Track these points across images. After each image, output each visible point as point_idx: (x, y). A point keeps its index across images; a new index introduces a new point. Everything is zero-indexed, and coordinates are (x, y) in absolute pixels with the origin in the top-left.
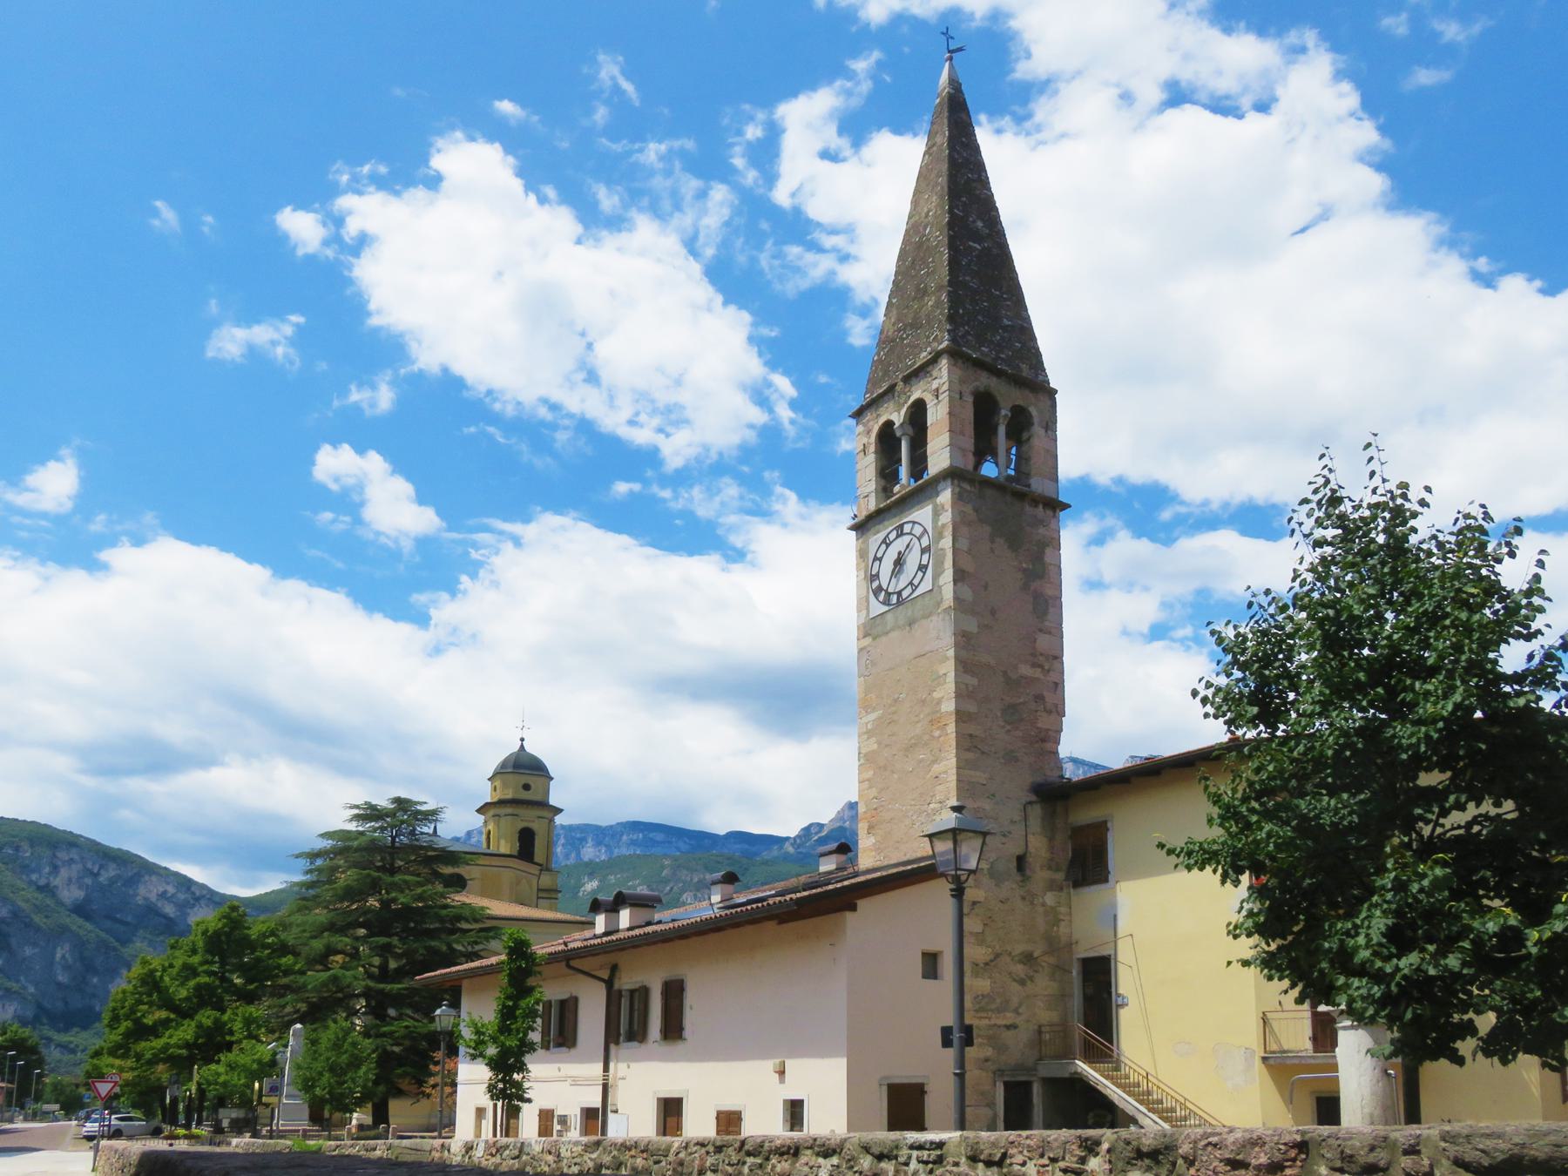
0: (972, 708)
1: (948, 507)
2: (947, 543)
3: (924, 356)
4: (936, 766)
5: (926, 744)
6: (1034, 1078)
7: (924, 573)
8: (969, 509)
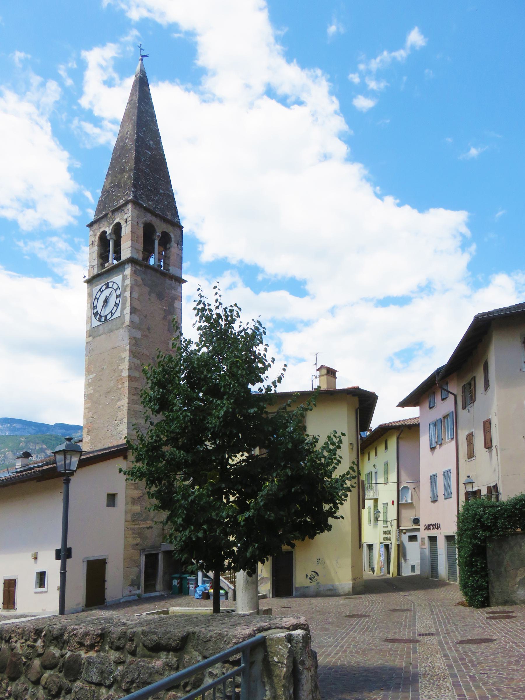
0: (137, 374)
1: (129, 276)
2: (128, 294)
3: (122, 202)
6: (160, 551)
7: (117, 308)
8: (139, 279)
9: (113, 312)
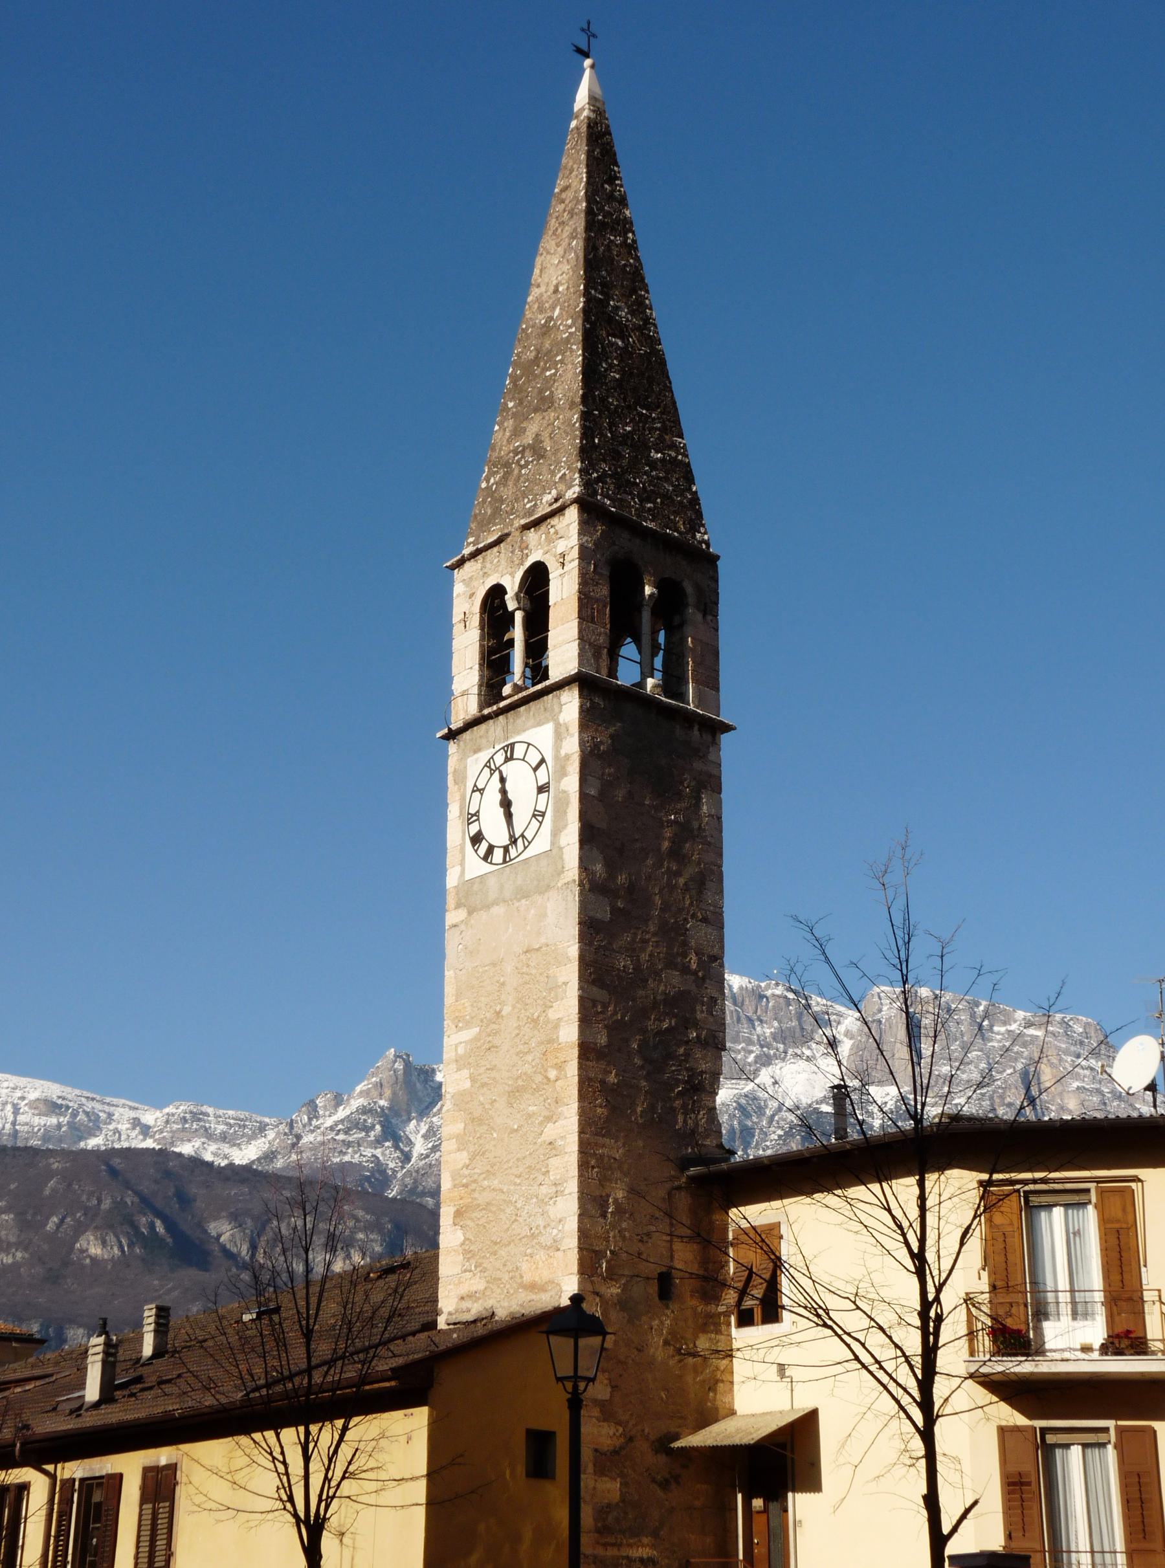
2: (571, 784)
4: (550, 1125)
5: (537, 1090)
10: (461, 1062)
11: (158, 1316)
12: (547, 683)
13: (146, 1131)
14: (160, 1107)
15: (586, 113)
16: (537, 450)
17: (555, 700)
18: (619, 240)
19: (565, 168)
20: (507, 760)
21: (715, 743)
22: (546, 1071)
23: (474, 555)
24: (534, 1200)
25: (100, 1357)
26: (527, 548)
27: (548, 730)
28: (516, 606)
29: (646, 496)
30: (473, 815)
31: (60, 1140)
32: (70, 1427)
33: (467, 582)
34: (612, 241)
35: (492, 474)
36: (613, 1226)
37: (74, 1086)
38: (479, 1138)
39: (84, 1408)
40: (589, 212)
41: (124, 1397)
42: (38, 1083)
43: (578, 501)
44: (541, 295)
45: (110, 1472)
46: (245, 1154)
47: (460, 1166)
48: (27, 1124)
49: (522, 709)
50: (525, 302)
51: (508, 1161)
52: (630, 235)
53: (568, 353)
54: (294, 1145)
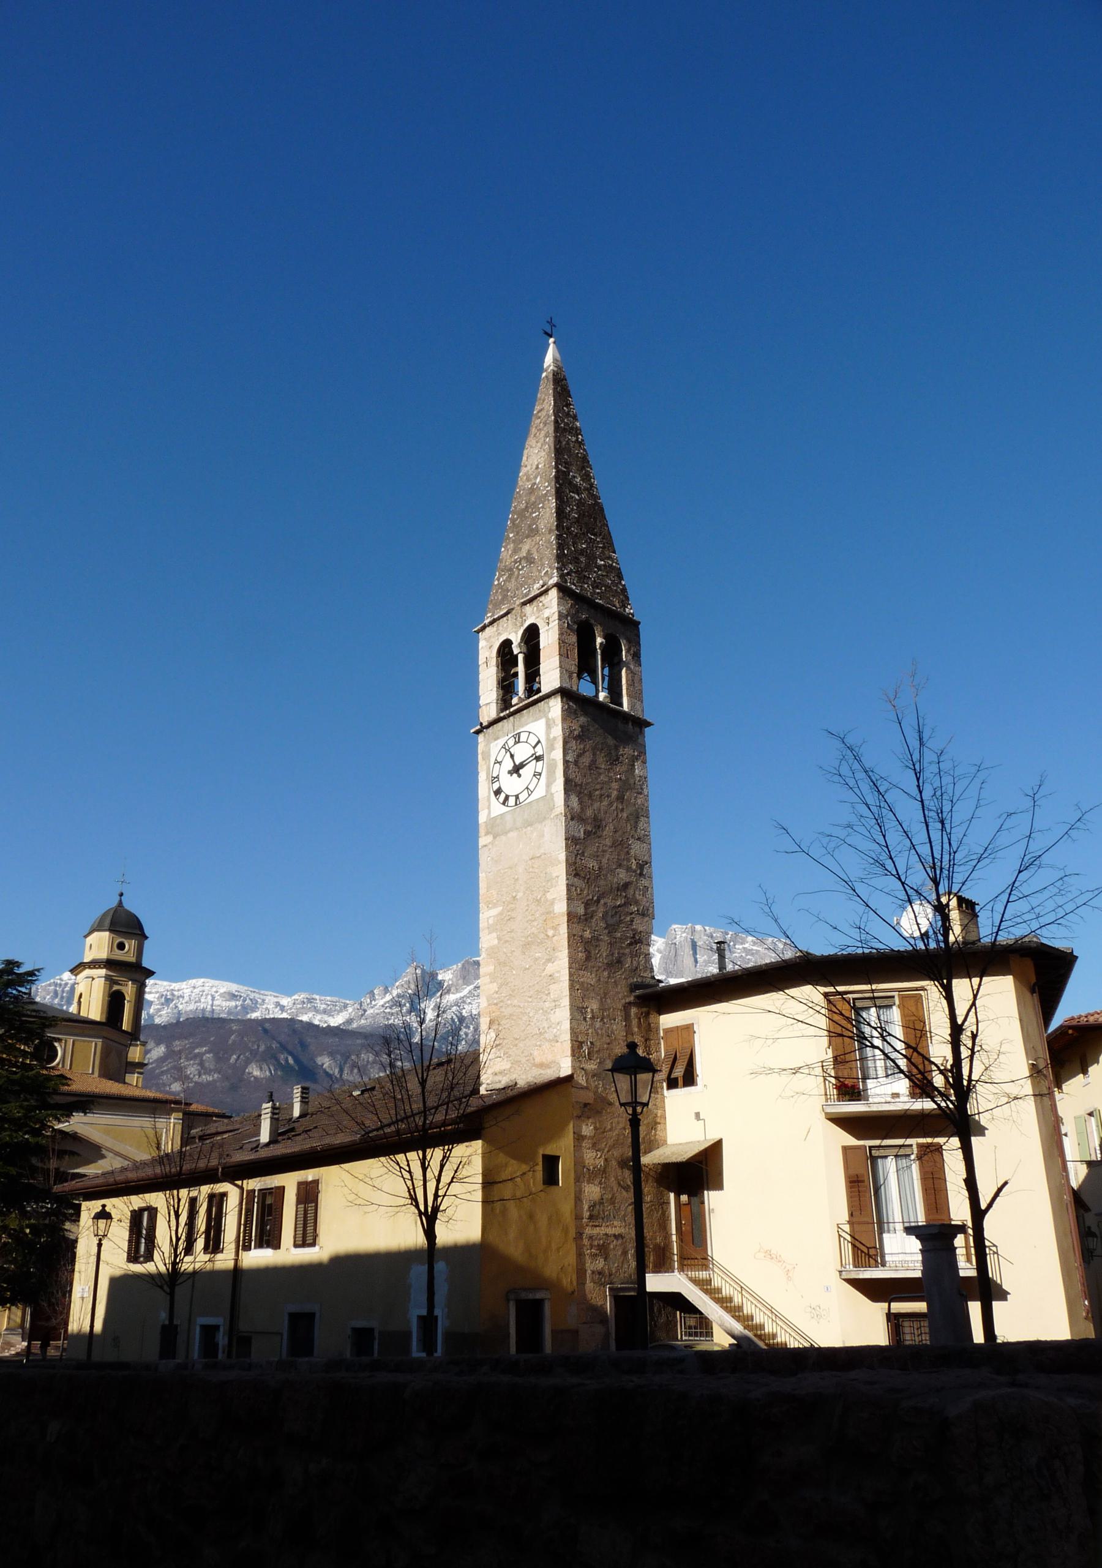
2: (558, 754)
3: (536, 589)
9: (531, 787)
10: (491, 929)
11: (302, 1093)
12: (541, 694)
13: (283, 1009)
14: (290, 996)
15: (551, 368)
16: (529, 559)
17: (546, 705)
18: (574, 439)
19: (540, 399)
20: (516, 743)
21: (642, 733)
22: (546, 931)
23: (491, 623)
24: (541, 1011)
25: (269, 1115)
26: (525, 616)
27: (542, 722)
28: (519, 651)
29: (596, 585)
30: (495, 778)
31: (237, 1014)
32: (251, 1158)
33: (487, 640)
34: (569, 439)
35: (501, 576)
36: (591, 1025)
37: (244, 985)
38: (505, 974)
39: (260, 1146)
40: (556, 422)
41: (284, 1139)
42: (225, 983)
43: (557, 585)
44: (528, 471)
45: (277, 1185)
46: (336, 1021)
47: (492, 992)
48: (219, 1006)
49: (525, 711)
50: (518, 476)
51: (523, 988)
52: (580, 436)
53: (547, 502)
54: (362, 1015)
